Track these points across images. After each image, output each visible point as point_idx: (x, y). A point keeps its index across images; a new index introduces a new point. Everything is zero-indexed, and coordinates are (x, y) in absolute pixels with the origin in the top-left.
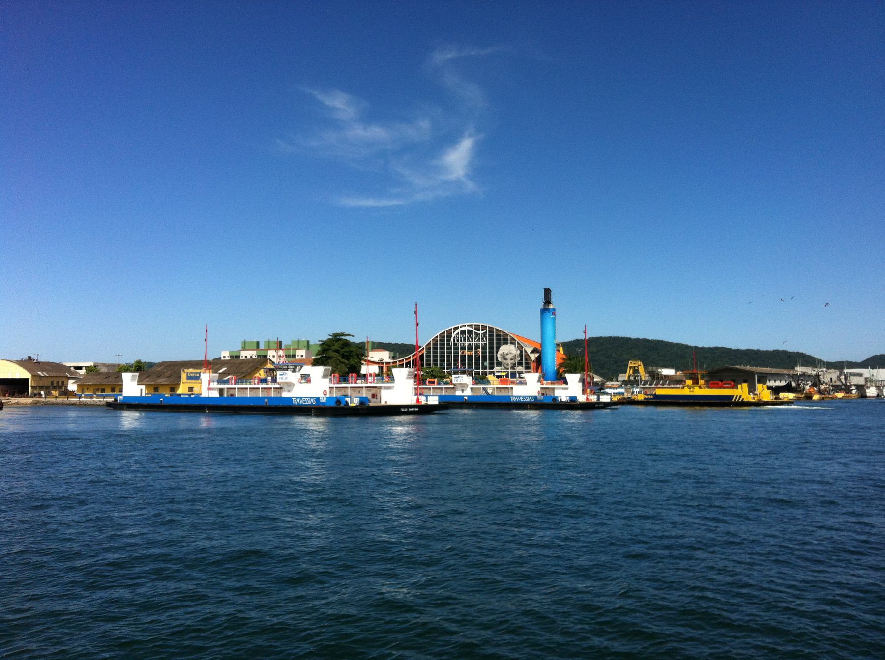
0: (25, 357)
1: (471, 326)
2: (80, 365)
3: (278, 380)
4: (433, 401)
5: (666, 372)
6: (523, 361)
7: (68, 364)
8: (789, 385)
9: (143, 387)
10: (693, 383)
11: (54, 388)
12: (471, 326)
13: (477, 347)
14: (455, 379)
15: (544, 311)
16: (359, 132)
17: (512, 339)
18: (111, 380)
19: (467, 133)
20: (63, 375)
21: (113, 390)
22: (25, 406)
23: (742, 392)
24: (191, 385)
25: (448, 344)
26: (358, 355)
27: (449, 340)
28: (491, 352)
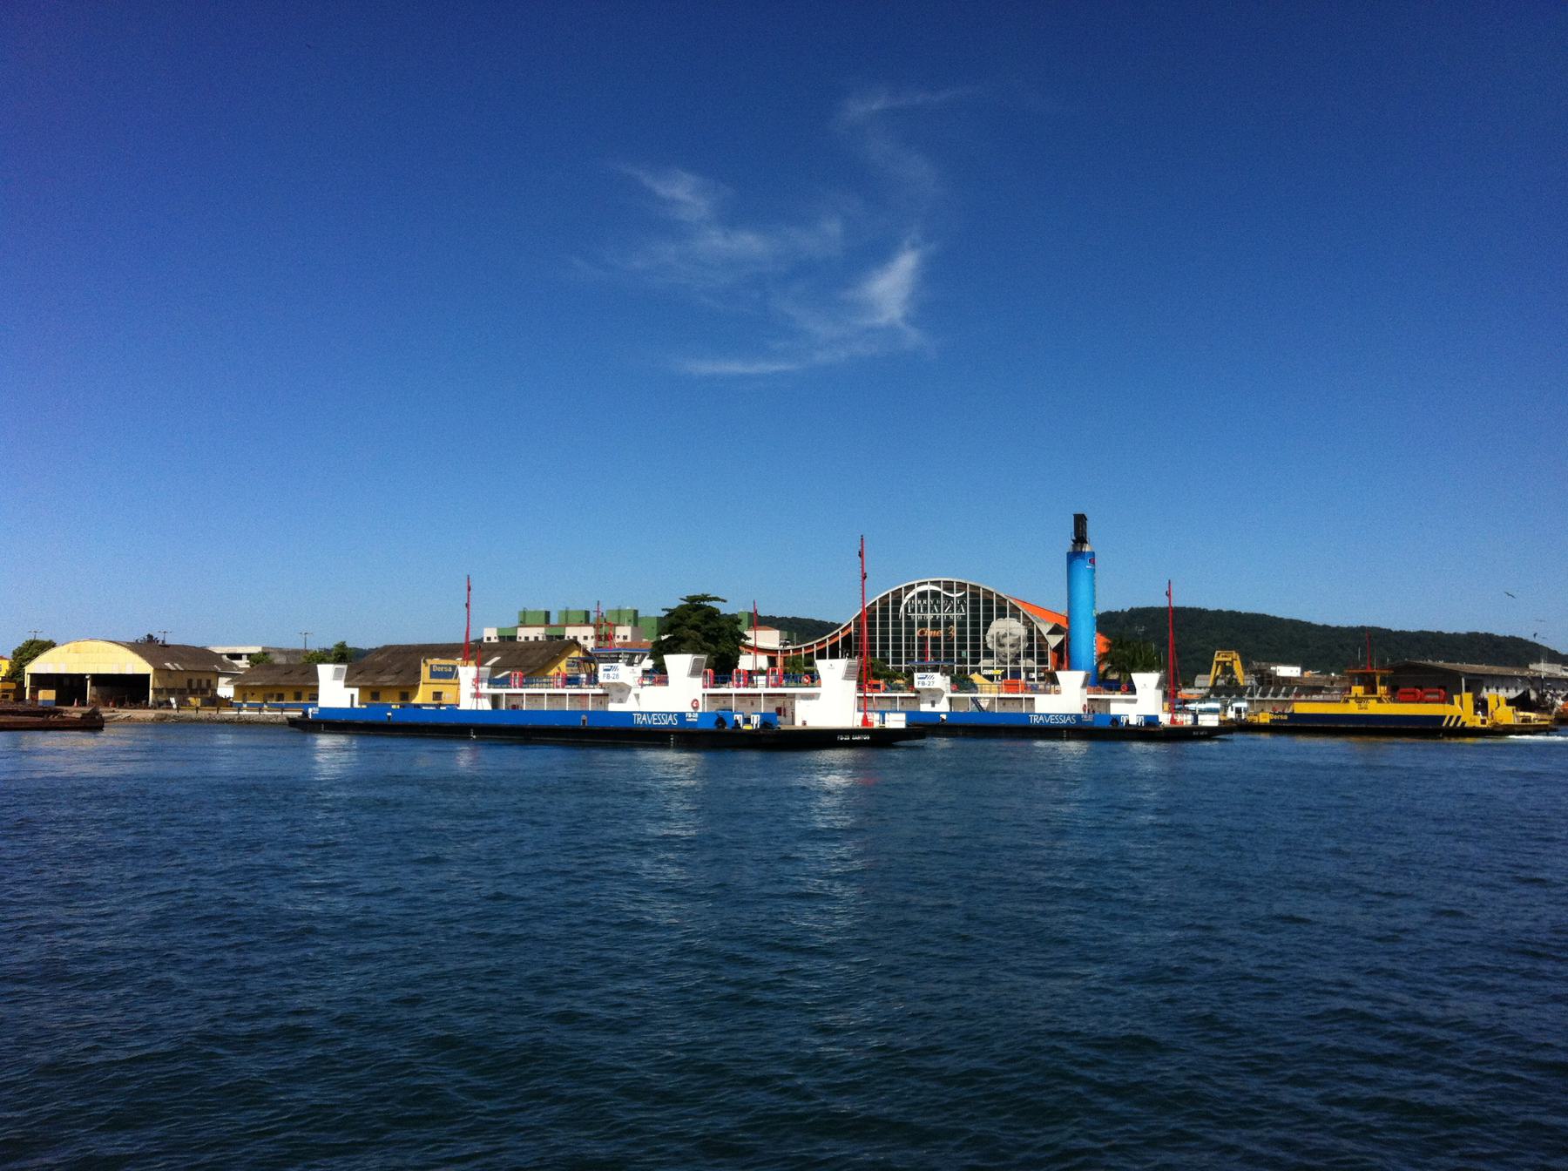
0: (141, 636)
1: (937, 583)
2: (239, 650)
3: (602, 678)
4: (896, 721)
5: (1285, 671)
6: (1034, 645)
7: (218, 650)
8: (1525, 696)
9: (356, 691)
10: (1366, 692)
11: (193, 693)
12: (937, 583)
13: (949, 623)
14: (919, 680)
15: (1075, 555)
16: (715, 242)
17: (1015, 609)
18: (295, 679)
19: (906, 243)
20: (209, 668)
21: (298, 696)
22: (142, 724)
23: (1461, 710)
24: (438, 688)
25: (896, 617)
26: (732, 636)
27: (896, 610)
28: (975, 632)
